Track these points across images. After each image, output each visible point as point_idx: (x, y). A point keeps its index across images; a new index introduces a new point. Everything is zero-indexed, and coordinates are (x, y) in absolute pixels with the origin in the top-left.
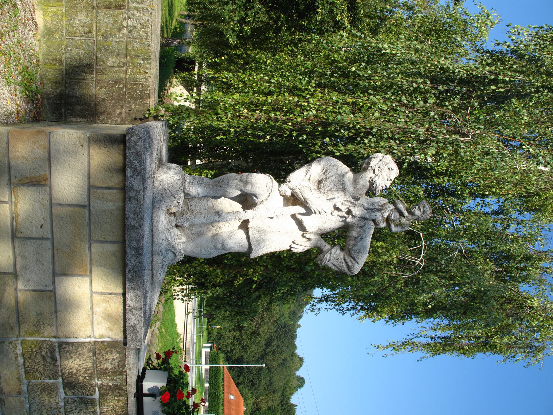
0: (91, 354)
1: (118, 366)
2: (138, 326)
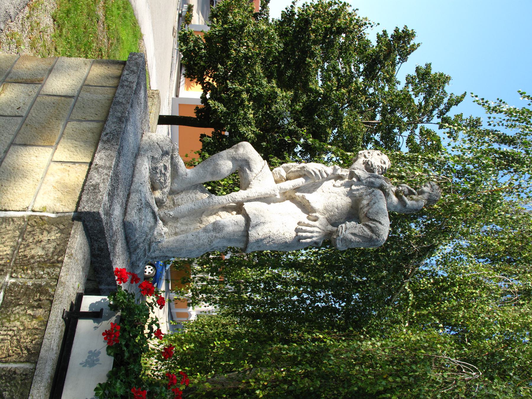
0: (18, 233)
1: (53, 253)
2: (101, 185)
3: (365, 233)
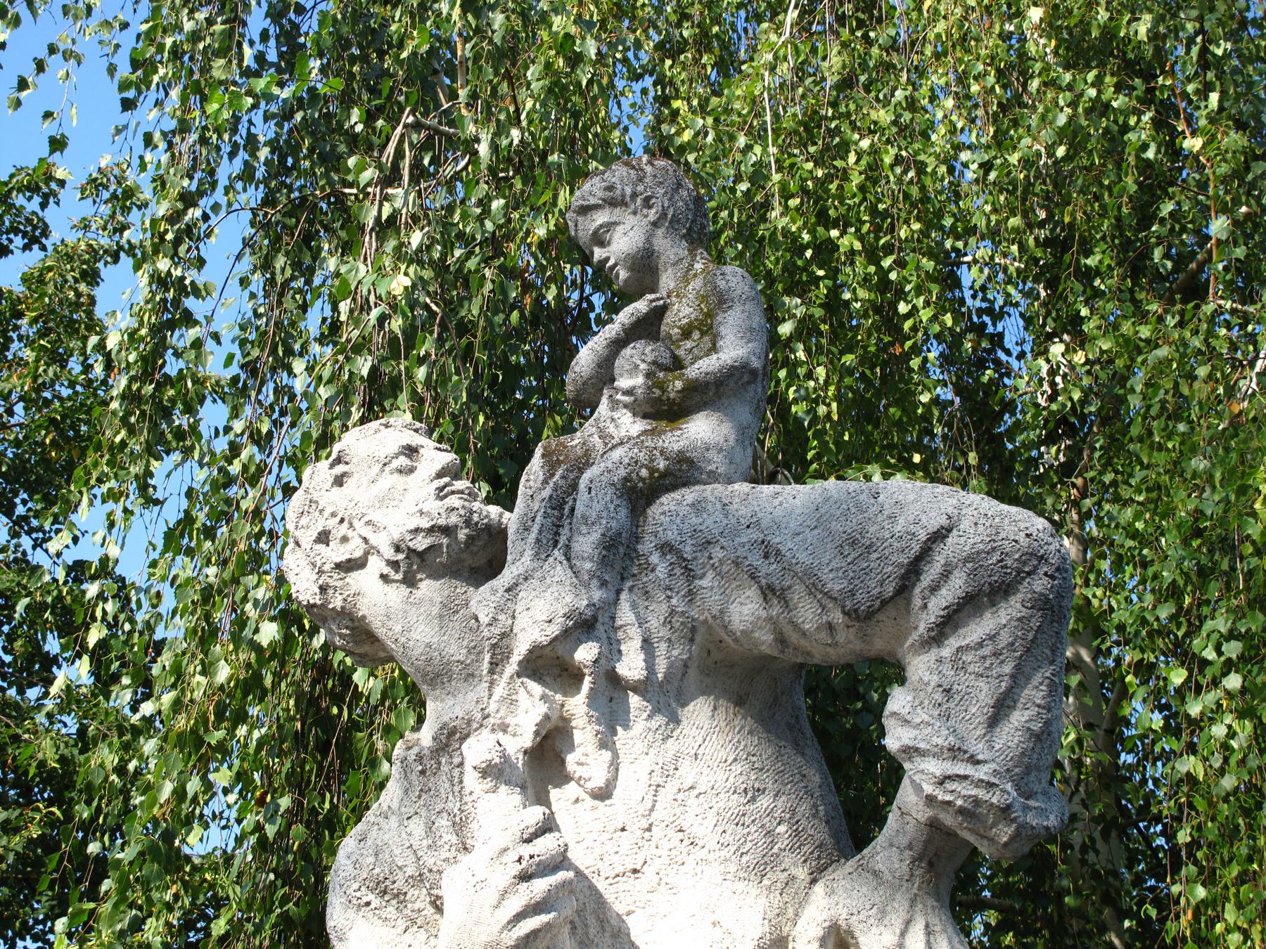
3: (1005, 638)
